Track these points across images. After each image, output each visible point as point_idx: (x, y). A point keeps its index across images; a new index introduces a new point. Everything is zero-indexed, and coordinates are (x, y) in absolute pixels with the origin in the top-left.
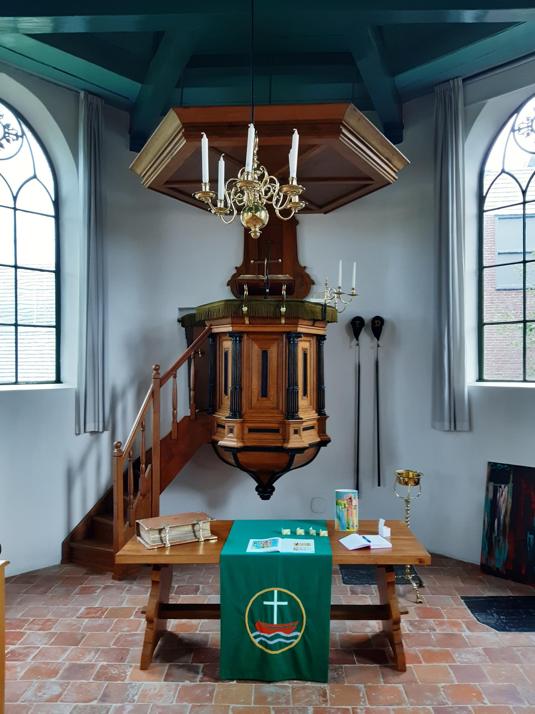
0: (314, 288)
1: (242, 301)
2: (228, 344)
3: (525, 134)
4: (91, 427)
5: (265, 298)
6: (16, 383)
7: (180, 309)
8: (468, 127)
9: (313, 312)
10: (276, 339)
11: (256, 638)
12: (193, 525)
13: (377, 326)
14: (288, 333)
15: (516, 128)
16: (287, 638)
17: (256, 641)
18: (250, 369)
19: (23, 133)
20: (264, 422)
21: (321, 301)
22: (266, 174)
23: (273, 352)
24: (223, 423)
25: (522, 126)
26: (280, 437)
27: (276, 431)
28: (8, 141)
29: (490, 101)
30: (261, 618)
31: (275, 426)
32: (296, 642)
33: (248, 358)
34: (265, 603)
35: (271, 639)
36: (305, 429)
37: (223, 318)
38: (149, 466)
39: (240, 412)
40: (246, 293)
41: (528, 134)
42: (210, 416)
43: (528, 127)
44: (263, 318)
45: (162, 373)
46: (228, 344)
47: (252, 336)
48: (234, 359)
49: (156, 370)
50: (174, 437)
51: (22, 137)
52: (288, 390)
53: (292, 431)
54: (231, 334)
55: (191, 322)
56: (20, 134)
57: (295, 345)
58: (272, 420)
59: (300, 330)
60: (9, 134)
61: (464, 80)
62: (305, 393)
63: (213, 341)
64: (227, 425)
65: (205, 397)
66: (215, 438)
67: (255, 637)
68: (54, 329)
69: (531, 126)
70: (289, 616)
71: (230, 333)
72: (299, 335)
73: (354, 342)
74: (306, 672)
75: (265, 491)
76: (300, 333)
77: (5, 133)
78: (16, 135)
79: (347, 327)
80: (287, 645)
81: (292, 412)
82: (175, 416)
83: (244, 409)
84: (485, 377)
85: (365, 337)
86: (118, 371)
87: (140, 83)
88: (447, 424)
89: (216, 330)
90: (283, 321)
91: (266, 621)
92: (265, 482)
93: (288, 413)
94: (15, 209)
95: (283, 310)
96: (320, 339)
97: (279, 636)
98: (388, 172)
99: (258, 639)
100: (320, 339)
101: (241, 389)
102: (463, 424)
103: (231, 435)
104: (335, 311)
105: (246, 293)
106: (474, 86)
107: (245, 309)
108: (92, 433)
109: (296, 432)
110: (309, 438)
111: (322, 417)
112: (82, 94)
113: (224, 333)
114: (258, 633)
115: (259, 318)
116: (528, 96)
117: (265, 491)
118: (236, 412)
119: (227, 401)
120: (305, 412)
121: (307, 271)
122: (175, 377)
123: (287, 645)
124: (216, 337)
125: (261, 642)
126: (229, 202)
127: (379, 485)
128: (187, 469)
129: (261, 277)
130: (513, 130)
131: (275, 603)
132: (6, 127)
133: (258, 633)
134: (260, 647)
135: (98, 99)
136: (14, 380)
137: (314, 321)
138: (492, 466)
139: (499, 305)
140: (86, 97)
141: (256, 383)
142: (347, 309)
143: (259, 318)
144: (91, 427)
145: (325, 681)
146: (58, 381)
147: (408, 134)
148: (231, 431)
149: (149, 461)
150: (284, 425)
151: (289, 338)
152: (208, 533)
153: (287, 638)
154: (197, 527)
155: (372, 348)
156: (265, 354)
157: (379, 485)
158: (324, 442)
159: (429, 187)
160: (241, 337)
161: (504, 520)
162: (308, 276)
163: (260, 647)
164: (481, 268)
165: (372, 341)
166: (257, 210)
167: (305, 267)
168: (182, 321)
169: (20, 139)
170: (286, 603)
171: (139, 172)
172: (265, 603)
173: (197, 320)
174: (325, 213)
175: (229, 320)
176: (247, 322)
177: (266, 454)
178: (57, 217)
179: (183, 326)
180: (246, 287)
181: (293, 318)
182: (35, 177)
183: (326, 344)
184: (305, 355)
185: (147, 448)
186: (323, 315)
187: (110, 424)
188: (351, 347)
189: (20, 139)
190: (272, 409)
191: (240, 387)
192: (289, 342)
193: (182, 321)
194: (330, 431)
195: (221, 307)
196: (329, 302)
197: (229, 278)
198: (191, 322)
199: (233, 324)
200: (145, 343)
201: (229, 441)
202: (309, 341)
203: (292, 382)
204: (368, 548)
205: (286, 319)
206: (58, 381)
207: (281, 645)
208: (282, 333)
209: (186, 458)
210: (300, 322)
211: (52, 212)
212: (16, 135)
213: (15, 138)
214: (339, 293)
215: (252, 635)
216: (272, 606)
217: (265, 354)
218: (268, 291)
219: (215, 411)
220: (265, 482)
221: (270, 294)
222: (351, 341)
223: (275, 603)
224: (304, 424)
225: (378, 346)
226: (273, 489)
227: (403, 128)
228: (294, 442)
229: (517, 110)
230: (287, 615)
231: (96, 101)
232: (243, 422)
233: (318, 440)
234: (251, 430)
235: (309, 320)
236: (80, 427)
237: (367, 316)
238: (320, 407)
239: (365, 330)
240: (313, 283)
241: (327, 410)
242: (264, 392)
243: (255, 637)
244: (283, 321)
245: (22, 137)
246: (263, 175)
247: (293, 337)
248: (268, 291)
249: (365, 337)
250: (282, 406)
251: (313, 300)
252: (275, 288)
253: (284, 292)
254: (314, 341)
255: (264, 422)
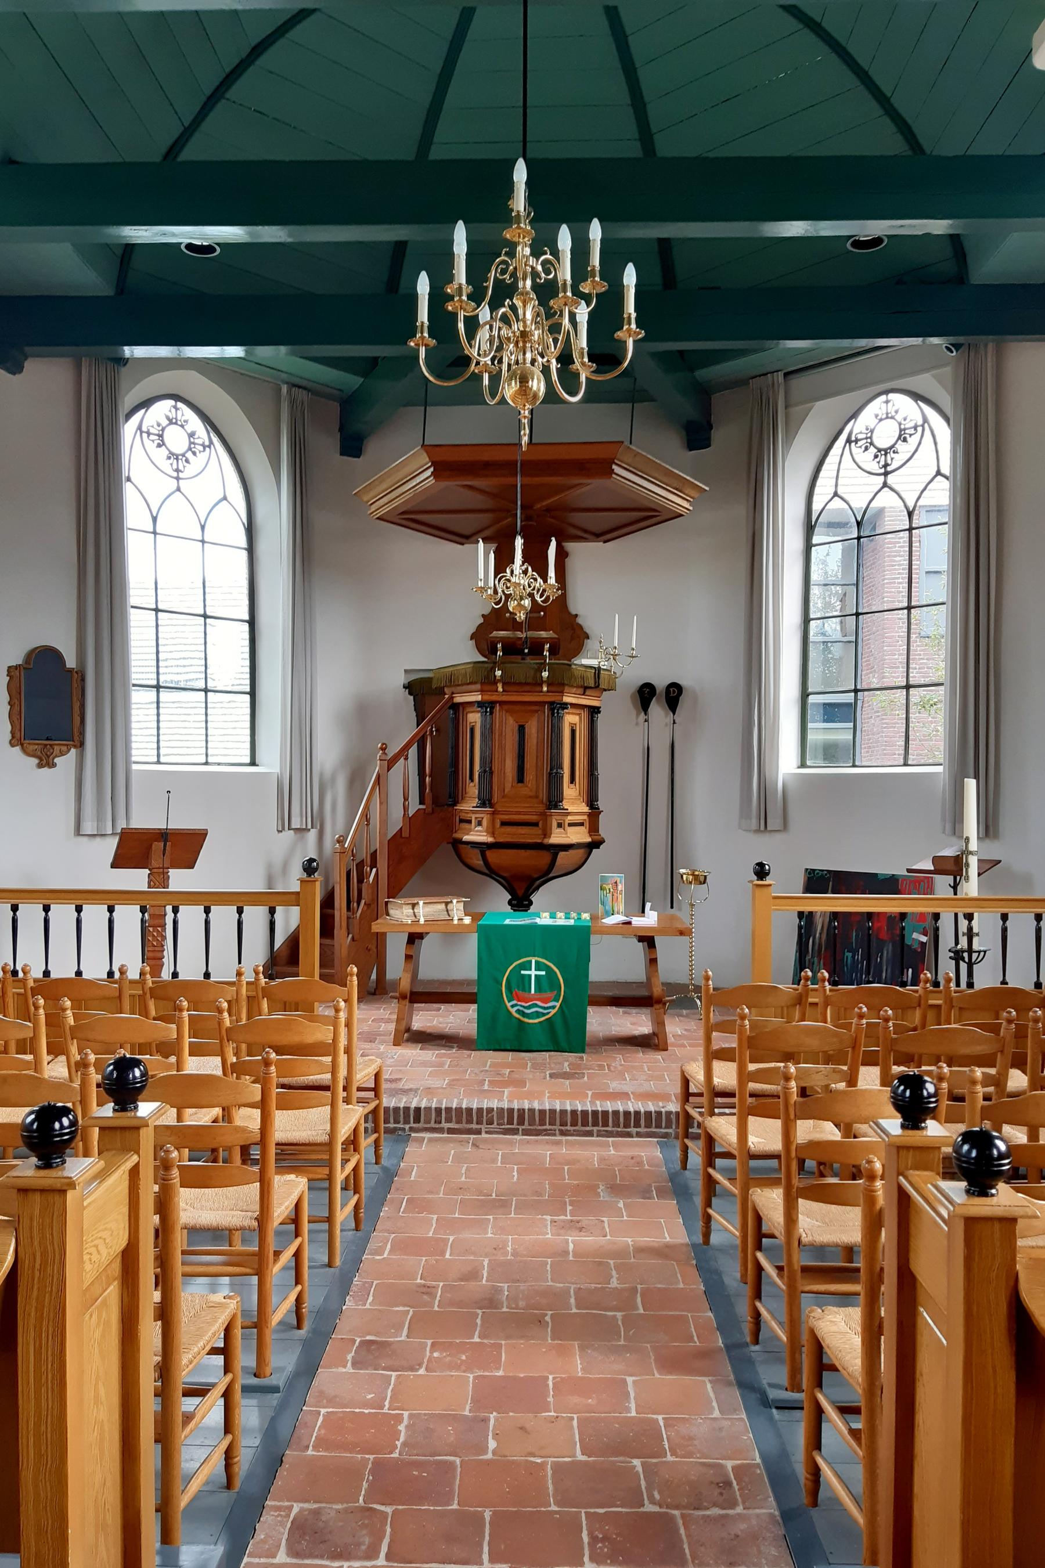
0: (589, 644)
1: (495, 663)
2: (474, 718)
3: (863, 448)
4: (296, 824)
5: (523, 659)
6: (207, 763)
7: (818, 882)
8: (789, 439)
9: (583, 678)
10: (537, 711)
11: (513, 1007)
12: (447, 904)
13: (674, 695)
14: (552, 703)
15: (853, 438)
16: (545, 1008)
17: (513, 1010)
18: (502, 747)
19: (211, 442)
20: (519, 813)
21: (594, 662)
22: (530, 569)
23: (532, 728)
24: (467, 816)
25: (860, 436)
26: (540, 832)
27: (536, 824)
28: (194, 453)
29: (819, 404)
30: (518, 987)
31: (534, 818)
32: (553, 1011)
33: (501, 735)
34: (523, 972)
35: (529, 1007)
36: (570, 825)
37: (471, 683)
38: (374, 870)
39: (490, 800)
40: (500, 653)
41: (905, 419)
42: (450, 809)
43: (867, 438)
44: (520, 684)
45: (392, 751)
46: (474, 718)
47: (505, 707)
48: (482, 734)
49: (382, 749)
50: (405, 834)
51: (209, 447)
52: (550, 774)
53: (555, 824)
54: (480, 704)
55: (423, 690)
56: (207, 443)
57: (560, 719)
58: (528, 811)
59: (567, 699)
60: (194, 443)
61: (786, 375)
62: (572, 780)
63: (455, 714)
64: (473, 816)
65: (441, 789)
66: (456, 835)
67: (513, 1006)
68: (810, 690)
69: (871, 438)
70: (547, 984)
71: (478, 702)
72: (564, 706)
73: (642, 716)
74: (564, 1044)
75: (521, 903)
76: (566, 704)
77: (191, 443)
78: (203, 445)
79: (632, 696)
80: (544, 1014)
81: (554, 801)
82: (406, 809)
83: (495, 799)
84: (808, 763)
85: (657, 709)
86: (329, 751)
87: (362, 376)
88: (754, 821)
89: (459, 699)
90: (545, 689)
91: (524, 990)
92: (520, 893)
93: (550, 802)
94: (203, 542)
95: (545, 674)
96: (594, 711)
97: (537, 1006)
98: (678, 502)
99: (516, 1008)
100: (594, 711)
101: (491, 773)
102: (774, 822)
103: (479, 828)
104: (613, 678)
105: (500, 653)
106: (799, 383)
107: (498, 673)
108: (297, 830)
109: (560, 825)
110: (579, 836)
111: (594, 812)
112: (285, 388)
113: (470, 704)
114: (515, 1002)
115: (515, 684)
116: (868, 398)
117: (521, 903)
118: (485, 801)
119: (473, 789)
120: (573, 804)
121: (579, 620)
122: (406, 759)
123: (544, 1014)
124: (456, 707)
125: (518, 1011)
126: (500, 591)
127: (672, 907)
128: (414, 881)
129: (519, 634)
130: (849, 441)
131: (533, 973)
132: (191, 435)
133: (515, 1002)
134: (517, 1016)
135: (305, 392)
136: (204, 761)
137: (585, 689)
138: (810, 873)
139: (925, 664)
140: (289, 392)
141: (510, 766)
142: (630, 674)
143: (515, 684)
144: (296, 824)
145: (583, 1052)
146: (253, 763)
147: (718, 436)
148: (480, 824)
149: (374, 865)
150: (545, 817)
151: (552, 710)
152: (462, 914)
153: (545, 1008)
154: (450, 907)
155: (666, 725)
156: (522, 729)
157: (672, 907)
158: (596, 844)
159: (741, 511)
160: (492, 708)
161: (820, 938)
162: (580, 627)
163: (517, 1016)
164: (806, 620)
165: (667, 715)
166: (522, 598)
167: (576, 615)
168: (410, 687)
169: (207, 449)
170: (543, 973)
171: (365, 499)
172: (523, 972)
173: (434, 686)
174: (605, 542)
175: (478, 686)
176: (500, 689)
177: (522, 853)
178: (251, 550)
179: (410, 693)
180: (499, 646)
181: (558, 684)
182: (225, 498)
183: (601, 718)
184: (573, 732)
185: (373, 850)
186: (597, 682)
187: (318, 822)
188: (637, 724)
189: (207, 449)
190: (530, 797)
191: (491, 769)
192: (553, 714)
193: (410, 687)
194: (603, 832)
195: (468, 671)
196: (604, 665)
197: (473, 630)
198: (423, 690)
199: (482, 691)
200: (362, 714)
201: (478, 835)
202: (579, 714)
203: (555, 764)
204: (629, 923)
205: (548, 686)
206: (253, 763)
207: (538, 1015)
208: (545, 703)
209: (421, 859)
210: (567, 689)
211: (243, 542)
212: (203, 445)
213: (201, 448)
214: (614, 655)
215: (509, 1005)
216: (530, 976)
217: (522, 729)
218: (526, 651)
219: (456, 802)
220: (520, 893)
221: (529, 654)
222: (638, 715)
223: (533, 973)
224: (569, 818)
225: (674, 723)
226: (531, 903)
227: (711, 427)
228: (557, 838)
229: (854, 416)
230: (545, 984)
231: (302, 395)
232: (493, 813)
233: (589, 840)
234: (504, 824)
235: (578, 687)
236: (284, 824)
237: (661, 683)
238: (592, 800)
239: (658, 701)
240: (588, 638)
241: (601, 804)
242: (521, 778)
243: (513, 1006)
244: (545, 689)
245: (209, 447)
246: (527, 569)
247: (557, 708)
248: (526, 651)
249: (657, 709)
250: (544, 795)
251: (585, 662)
252: (536, 648)
253: (546, 653)
254: (585, 714)
255: (519, 813)
